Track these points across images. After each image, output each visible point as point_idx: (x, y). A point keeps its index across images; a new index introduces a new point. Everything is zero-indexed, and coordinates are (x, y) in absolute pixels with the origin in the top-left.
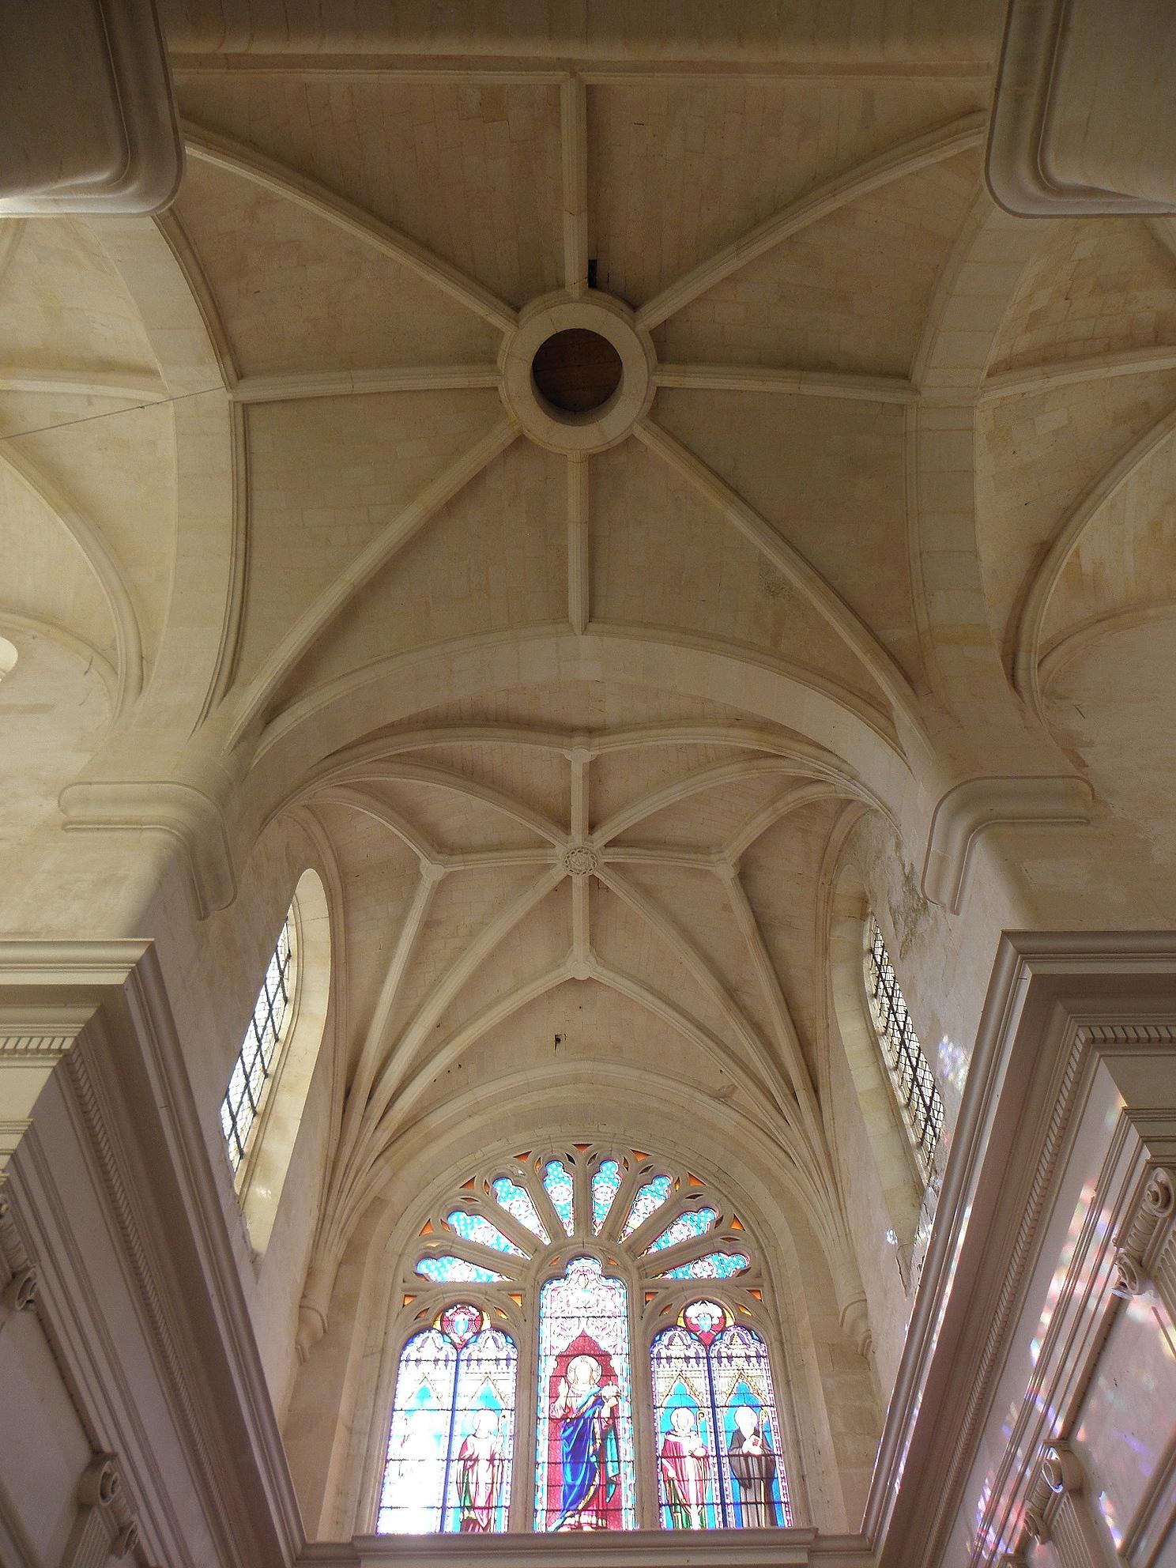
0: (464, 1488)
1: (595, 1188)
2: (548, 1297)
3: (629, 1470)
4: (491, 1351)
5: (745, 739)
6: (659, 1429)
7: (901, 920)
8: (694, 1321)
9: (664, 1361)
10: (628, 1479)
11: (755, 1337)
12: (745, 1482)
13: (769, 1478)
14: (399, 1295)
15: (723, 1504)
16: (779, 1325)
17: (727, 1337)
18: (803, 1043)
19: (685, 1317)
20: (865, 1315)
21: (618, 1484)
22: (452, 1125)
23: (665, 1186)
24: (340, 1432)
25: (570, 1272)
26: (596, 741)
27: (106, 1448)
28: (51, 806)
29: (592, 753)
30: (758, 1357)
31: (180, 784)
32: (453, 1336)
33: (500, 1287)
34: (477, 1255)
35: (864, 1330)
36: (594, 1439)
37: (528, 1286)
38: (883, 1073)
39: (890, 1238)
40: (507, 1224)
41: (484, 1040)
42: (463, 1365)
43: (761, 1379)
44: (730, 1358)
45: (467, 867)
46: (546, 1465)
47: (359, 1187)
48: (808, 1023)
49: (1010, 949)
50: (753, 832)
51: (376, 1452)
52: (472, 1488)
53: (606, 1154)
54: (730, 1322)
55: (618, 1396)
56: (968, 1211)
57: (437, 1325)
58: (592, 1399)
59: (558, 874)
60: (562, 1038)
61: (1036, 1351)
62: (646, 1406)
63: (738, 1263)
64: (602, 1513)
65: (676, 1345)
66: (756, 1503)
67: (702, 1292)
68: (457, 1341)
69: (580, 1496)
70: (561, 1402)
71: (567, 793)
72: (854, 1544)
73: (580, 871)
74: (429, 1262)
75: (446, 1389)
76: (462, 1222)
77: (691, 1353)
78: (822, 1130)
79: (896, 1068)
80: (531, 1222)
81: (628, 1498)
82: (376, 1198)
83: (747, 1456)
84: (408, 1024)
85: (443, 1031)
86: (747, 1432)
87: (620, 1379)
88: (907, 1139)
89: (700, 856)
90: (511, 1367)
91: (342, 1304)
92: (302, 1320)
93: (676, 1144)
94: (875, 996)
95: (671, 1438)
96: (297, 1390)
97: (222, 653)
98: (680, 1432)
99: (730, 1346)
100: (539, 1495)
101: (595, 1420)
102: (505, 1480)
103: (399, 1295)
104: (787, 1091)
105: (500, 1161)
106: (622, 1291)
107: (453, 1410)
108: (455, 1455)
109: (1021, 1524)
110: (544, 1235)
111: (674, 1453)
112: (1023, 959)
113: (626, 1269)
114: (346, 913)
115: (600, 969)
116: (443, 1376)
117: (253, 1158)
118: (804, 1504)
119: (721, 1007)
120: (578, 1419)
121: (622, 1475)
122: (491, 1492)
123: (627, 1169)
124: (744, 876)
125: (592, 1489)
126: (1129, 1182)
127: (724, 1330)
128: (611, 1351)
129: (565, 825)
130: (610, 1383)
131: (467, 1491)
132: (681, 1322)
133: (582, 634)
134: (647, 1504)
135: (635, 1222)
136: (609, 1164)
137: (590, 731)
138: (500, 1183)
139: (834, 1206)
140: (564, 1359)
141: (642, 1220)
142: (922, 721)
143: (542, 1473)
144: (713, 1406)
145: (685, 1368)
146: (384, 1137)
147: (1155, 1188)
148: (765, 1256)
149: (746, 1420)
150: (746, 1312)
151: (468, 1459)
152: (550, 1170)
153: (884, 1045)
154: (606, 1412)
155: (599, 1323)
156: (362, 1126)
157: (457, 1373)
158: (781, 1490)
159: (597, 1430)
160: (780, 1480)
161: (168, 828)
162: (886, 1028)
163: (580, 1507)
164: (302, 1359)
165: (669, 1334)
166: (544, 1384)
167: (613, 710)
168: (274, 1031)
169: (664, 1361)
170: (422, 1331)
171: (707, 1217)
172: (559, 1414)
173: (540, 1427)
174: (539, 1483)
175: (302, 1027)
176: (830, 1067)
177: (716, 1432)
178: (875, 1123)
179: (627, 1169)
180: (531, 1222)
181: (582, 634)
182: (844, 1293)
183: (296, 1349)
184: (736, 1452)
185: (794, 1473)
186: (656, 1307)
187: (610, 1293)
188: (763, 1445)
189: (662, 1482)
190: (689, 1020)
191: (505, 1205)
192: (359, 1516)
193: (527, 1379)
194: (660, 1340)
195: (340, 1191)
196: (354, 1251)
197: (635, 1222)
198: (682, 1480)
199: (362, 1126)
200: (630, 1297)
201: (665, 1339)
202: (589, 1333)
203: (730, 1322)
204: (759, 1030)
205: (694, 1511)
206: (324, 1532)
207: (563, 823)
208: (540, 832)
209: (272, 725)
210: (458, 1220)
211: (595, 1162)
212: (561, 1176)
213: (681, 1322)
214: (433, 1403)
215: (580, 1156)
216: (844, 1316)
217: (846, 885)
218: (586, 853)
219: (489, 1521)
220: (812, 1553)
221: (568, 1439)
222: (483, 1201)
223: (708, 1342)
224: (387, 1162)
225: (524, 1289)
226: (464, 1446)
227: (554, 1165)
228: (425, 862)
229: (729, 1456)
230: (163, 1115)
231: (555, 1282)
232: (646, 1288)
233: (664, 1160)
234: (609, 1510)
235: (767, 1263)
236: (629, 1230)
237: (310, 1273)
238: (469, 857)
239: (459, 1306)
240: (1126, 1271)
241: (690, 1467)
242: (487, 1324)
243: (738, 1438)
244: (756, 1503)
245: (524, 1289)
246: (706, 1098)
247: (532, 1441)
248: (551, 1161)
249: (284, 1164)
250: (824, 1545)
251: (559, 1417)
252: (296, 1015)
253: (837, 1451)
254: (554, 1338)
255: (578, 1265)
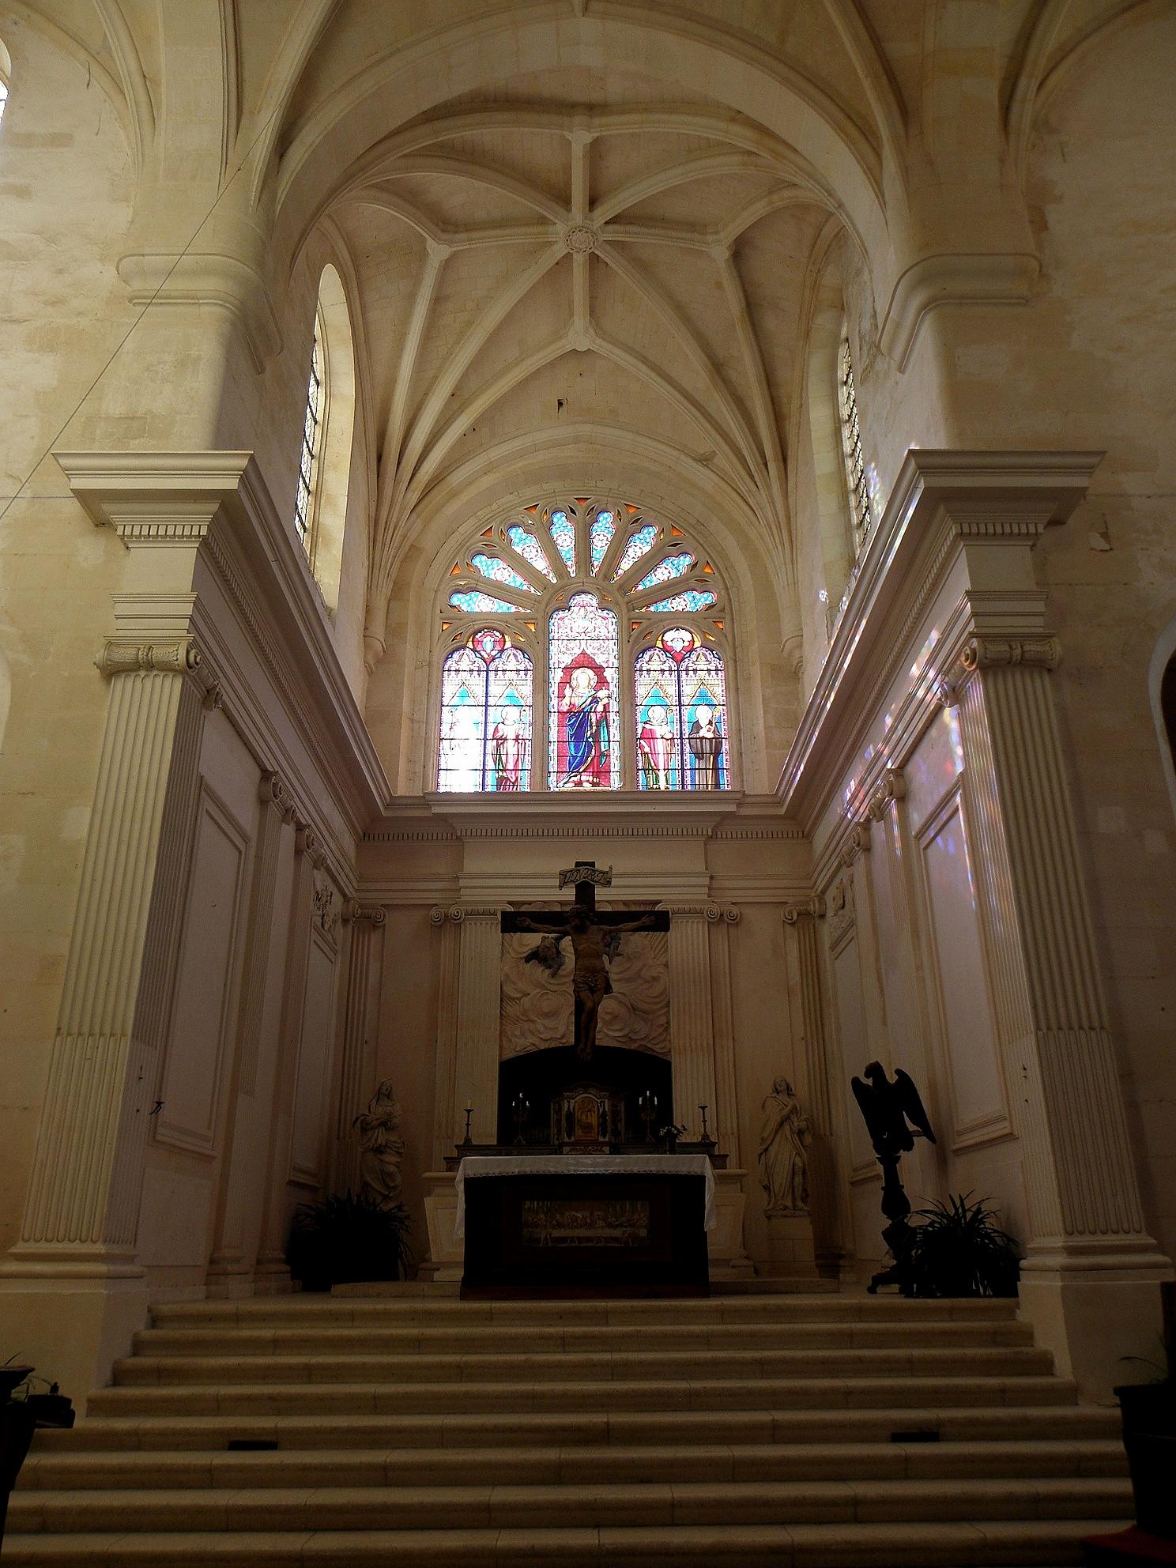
0: (498, 759)
1: (593, 536)
2: (556, 624)
3: (616, 748)
4: (512, 664)
5: (742, 136)
6: (639, 720)
7: (865, 348)
8: (669, 644)
9: (645, 673)
10: (615, 751)
11: (716, 655)
12: (699, 755)
13: (717, 753)
14: (438, 622)
15: (683, 769)
16: (735, 648)
17: (694, 657)
18: (779, 418)
19: (662, 640)
20: (800, 646)
21: (608, 756)
22: (470, 482)
23: (652, 534)
24: (405, 722)
25: (573, 605)
26: (597, 121)
27: (304, 822)
28: (107, 276)
29: (592, 135)
30: (717, 670)
31: (222, 255)
32: (483, 653)
33: (517, 617)
34: (497, 590)
35: (797, 657)
36: (591, 726)
37: (540, 618)
38: (841, 459)
39: (823, 595)
40: (519, 564)
41: (498, 406)
42: (492, 674)
43: (717, 687)
44: (695, 671)
45: (472, 246)
46: (556, 743)
47: (397, 539)
48: (785, 400)
49: (913, 463)
50: (747, 219)
51: (433, 735)
52: (504, 757)
53: (604, 506)
54: (697, 644)
55: (609, 697)
56: (864, 622)
57: (470, 645)
58: (590, 699)
59: (559, 250)
60: (565, 403)
61: (889, 721)
62: (629, 705)
63: (708, 598)
64: (596, 774)
65: (655, 661)
66: (706, 769)
67: (677, 621)
68: (486, 656)
69: (581, 763)
70: (566, 701)
71: (567, 169)
72: (770, 800)
73: (581, 249)
74: (460, 596)
75: (480, 691)
76: (484, 563)
77: (666, 667)
78: (785, 495)
79: (852, 455)
80: (541, 564)
81: (615, 765)
82: (412, 546)
83: (702, 738)
84: (426, 394)
85: (458, 400)
86: (703, 722)
87: (611, 685)
88: (850, 520)
89: (696, 236)
90: (528, 676)
91: (395, 630)
92: (367, 646)
93: (662, 498)
94: (846, 383)
95: (648, 726)
96: (369, 693)
97: (226, 79)
98: (654, 723)
99: (696, 663)
100: (552, 763)
101: (592, 714)
102: (527, 753)
103: (438, 622)
104: (759, 459)
105: (513, 512)
106: (614, 620)
107: (486, 706)
108: (490, 736)
109: (867, 812)
110: (551, 575)
111: (649, 736)
112: (921, 473)
113: (617, 603)
114: (361, 294)
115: (599, 341)
116: (477, 684)
117: (315, 530)
118: (739, 773)
119: (708, 381)
120: (579, 712)
121: (611, 749)
122: (518, 760)
123: (620, 520)
124: (739, 252)
125: (590, 759)
126: (960, 637)
127: (692, 650)
128: (605, 665)
129: (566, 201)
130: (604, 688)
131: (500, 759)
132: (659, 644)
133: (583, 16)
134: (629, 770)
135: (626, 565)
136: (606, 515)
137: (593, 109)
138: (514, 530)
139: (788, 560)
140: (568, 670)
141: (632, 564)
142: (905, 171)
143: (553, 748)
144: (680, 705)
145: (660, 678)
146: (414, 497)
147: (968, 652)
148: (729, 595)
149: (703, 715)
150: (711, 638)
151: (499, 739)
152: (555, 520)
153: (846, 433)
154: (600, 708)
155: (596, 644)
156: (395, 487)
157: (487, 680)
158: (725, 761)
159: (594, 720)
160: (724, 754)
161: (221, 303)
162: (850, 416)
163: (581, 771)
164: (370, 672)
165: (649, 653)
166: (554, 688)
167: (614, 89)
168: (312, 414)
169: (645, 673)
170: (457, 649)
171: (686, 561)
172: (565, 709)
173: (551, 749)
174: (552, 755)
175: (335, 408)
176: (798, 442)
177: (681, 722)
178: (826, 504)
179: (620, 520)
180: (541, 564)
181: (583, 16)
182: (787, 629)
183: (365, 666)
184: (695, 736)
185: (735, 751)
186: (639, 634)
187: (605, 622)
188: (714, 731)
189: (640, 755)
190: (679, 391)
191: (518, 550)
192: (425, 776)
193: (541, 684)
194: (642, 657)
195: (383, 544)
196: (399, 590)
197: (626, 565)
198: (654, 753)
199: (395, 487)
200: (619, 624)
201: (646, 657)
202: (588, 652)
203: (697, 644)
204: (740, 403)
205: (662, 774)
206: (402, 789)
207: (564, 199)
208: (541, 211)
209: (287, 159)
210: (480, 562)
211: (593, 514)
212: (565, 525)
213: (659, 644)
214: (471, 701)
215: (580, 508)
216: (784, 646)
217: (830, 278)
218: (587, 232)
219: (517, 779)
220: (739, 805)
221: (572, 726)
222: (500, 547)
223: (678, 658)
224: (418, 517)
225: (536, 619)
226: (496, 730)
227: (559, 515)
228: (431, 243)
229: (689, 738)
230: (274, 565)
231: (561, 612)
232: (633, 619)
233: (652, 513)
234: (601, 773)
235: (730, 600)
236: (620, 572)
237: (368, 610)
238: (475, 235)
239: (485, 630)
240: (945, 695)
241: (660, 746)
242: (508, 644)
243: (697, 726)
244: (706, 769)
245: (536, 619)
246: (691, 461)
247: (546, 727)
248: (556, 512)
249: (340, 536)
250: (749, 800)
251: (565, 710)
252: (328, 396)
253: (767, 738)
254: (560, 655)
255: (578, 599)
